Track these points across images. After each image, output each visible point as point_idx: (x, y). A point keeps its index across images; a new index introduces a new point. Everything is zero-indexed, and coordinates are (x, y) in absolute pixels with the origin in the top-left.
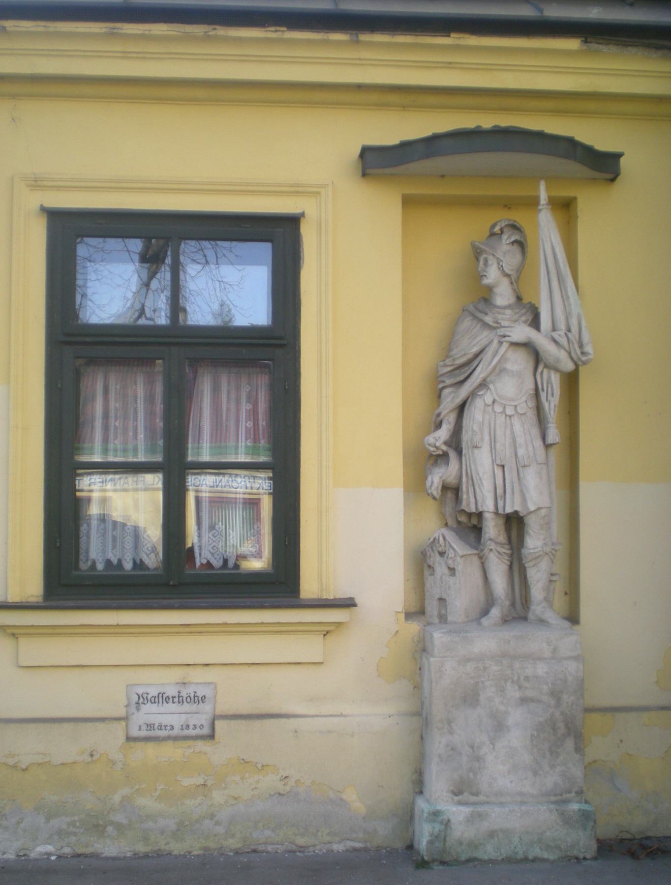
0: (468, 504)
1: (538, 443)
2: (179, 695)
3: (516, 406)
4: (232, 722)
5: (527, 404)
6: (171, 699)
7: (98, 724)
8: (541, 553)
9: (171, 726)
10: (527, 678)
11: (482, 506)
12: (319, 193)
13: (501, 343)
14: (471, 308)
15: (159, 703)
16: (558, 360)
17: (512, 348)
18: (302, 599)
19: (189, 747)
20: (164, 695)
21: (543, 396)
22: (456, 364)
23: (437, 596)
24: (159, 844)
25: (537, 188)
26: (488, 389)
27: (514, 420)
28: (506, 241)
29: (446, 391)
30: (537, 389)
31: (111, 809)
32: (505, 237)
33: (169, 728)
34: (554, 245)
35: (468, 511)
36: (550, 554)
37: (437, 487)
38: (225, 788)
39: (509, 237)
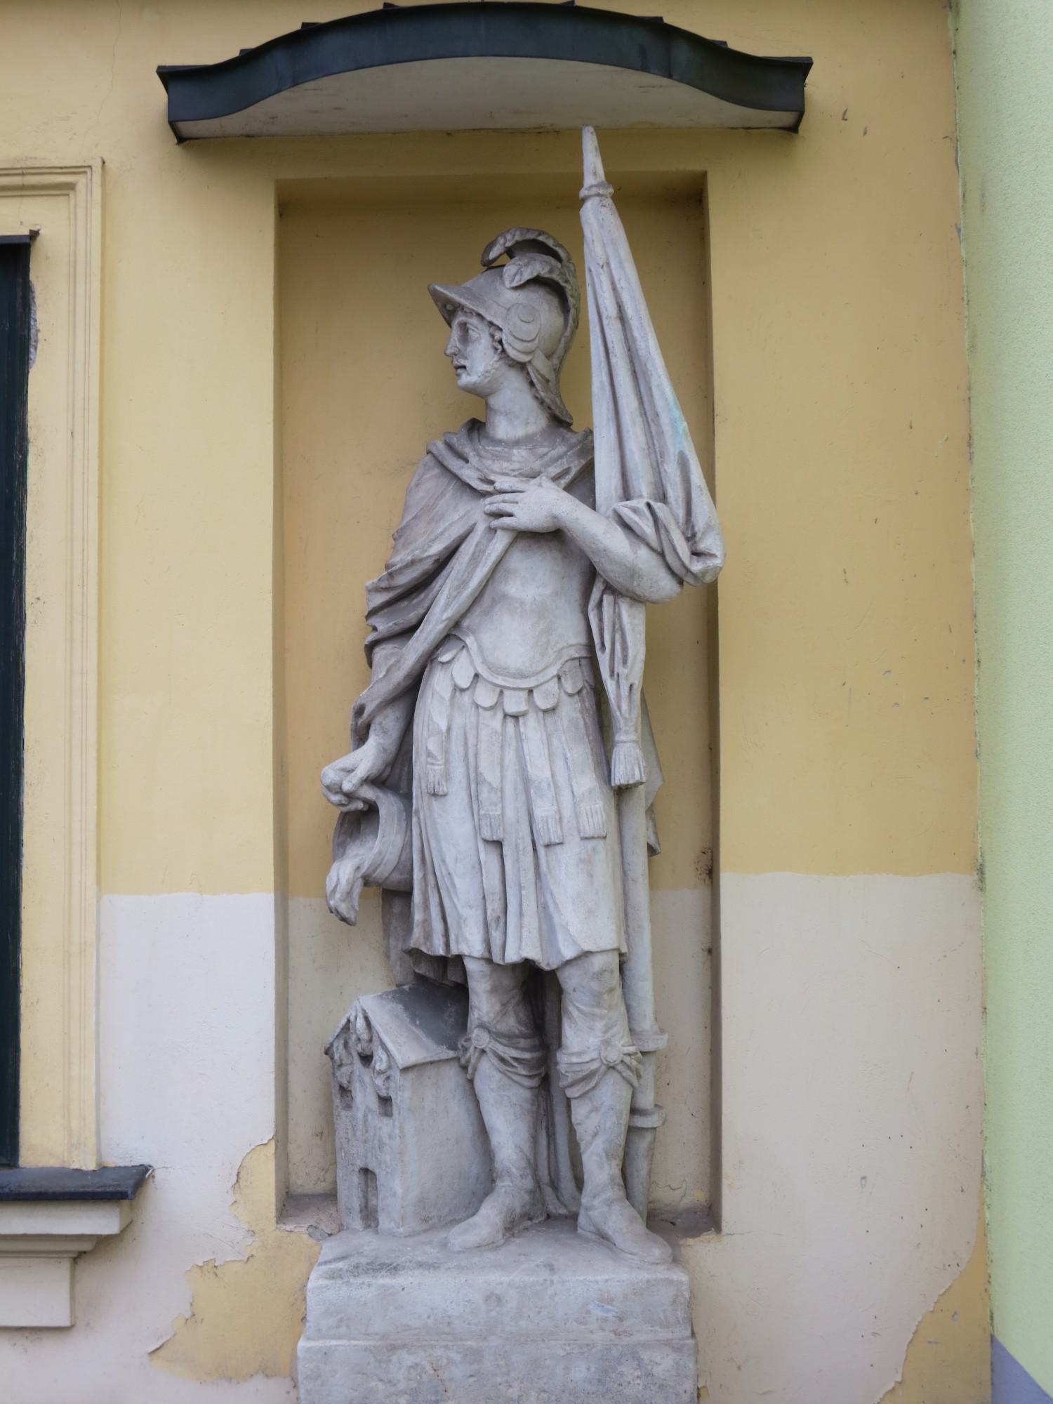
0: (428, 936)
1: (587, 781)
3: (531, 691)
8: (594, 1066)
11: (457, 942)
14: (440, 448)
16: (633, 573)
21: (603, 660)
23: (360, 1163)
26: (464, 647)
30: (590, 646)
34: (617, 282)
36: (619, 1067)
37: (349, 893)
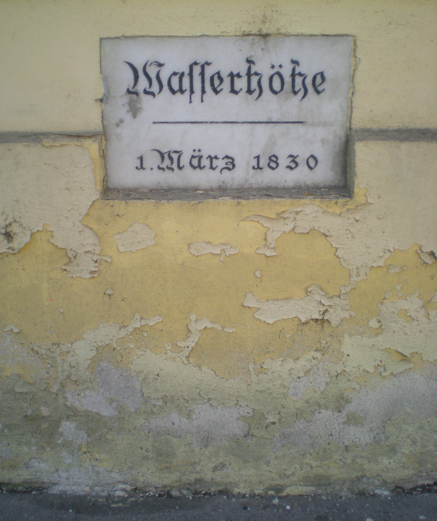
2: (249, 69)
4: (405, 146)
6: (227, 81)
7: (19, 148)
9: (227, 157)
15: (192, 92)
19: (280, 217)
20: (207, 68)
24: (198, 468)
31: (69, 377)
33: (220, 163)
38: (379, 331)
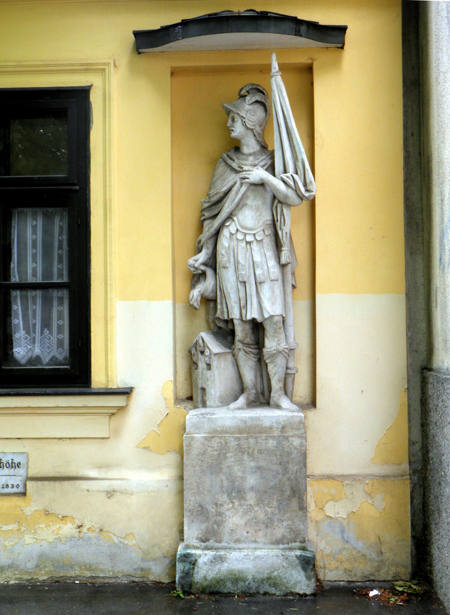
0: (222, 313)
5: (264, 233)
10: (260, 451)
11: (231, 314)
12: (104, 70)
13: (242, 184)
16: (286, 197)
17: (252, 187)
18: (93, 388)
22: (212, 201)
25: (270, 58)
27: (253, 245)
28: (249, 102)
29: (206, 223)
32: (248, 98)
35: (223, 319)
36: (283, 352)
39: (251, 99)
